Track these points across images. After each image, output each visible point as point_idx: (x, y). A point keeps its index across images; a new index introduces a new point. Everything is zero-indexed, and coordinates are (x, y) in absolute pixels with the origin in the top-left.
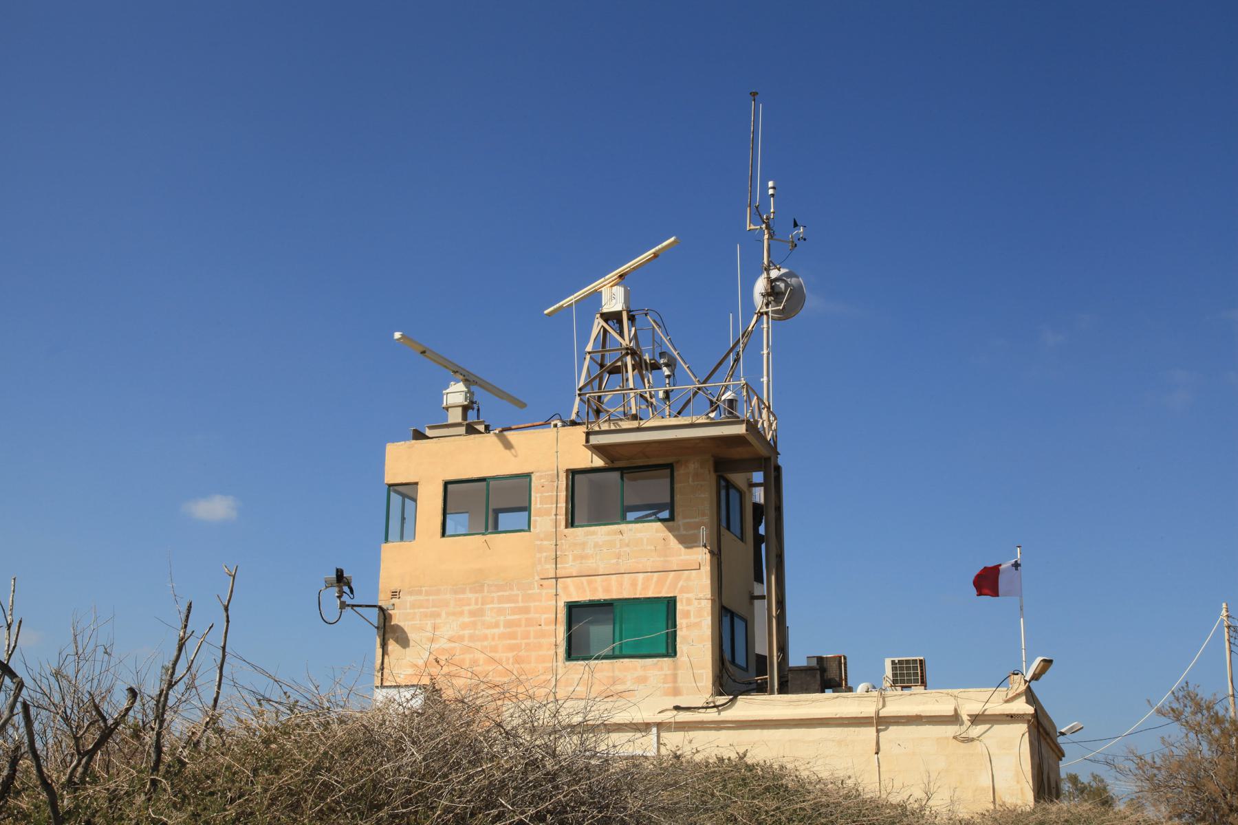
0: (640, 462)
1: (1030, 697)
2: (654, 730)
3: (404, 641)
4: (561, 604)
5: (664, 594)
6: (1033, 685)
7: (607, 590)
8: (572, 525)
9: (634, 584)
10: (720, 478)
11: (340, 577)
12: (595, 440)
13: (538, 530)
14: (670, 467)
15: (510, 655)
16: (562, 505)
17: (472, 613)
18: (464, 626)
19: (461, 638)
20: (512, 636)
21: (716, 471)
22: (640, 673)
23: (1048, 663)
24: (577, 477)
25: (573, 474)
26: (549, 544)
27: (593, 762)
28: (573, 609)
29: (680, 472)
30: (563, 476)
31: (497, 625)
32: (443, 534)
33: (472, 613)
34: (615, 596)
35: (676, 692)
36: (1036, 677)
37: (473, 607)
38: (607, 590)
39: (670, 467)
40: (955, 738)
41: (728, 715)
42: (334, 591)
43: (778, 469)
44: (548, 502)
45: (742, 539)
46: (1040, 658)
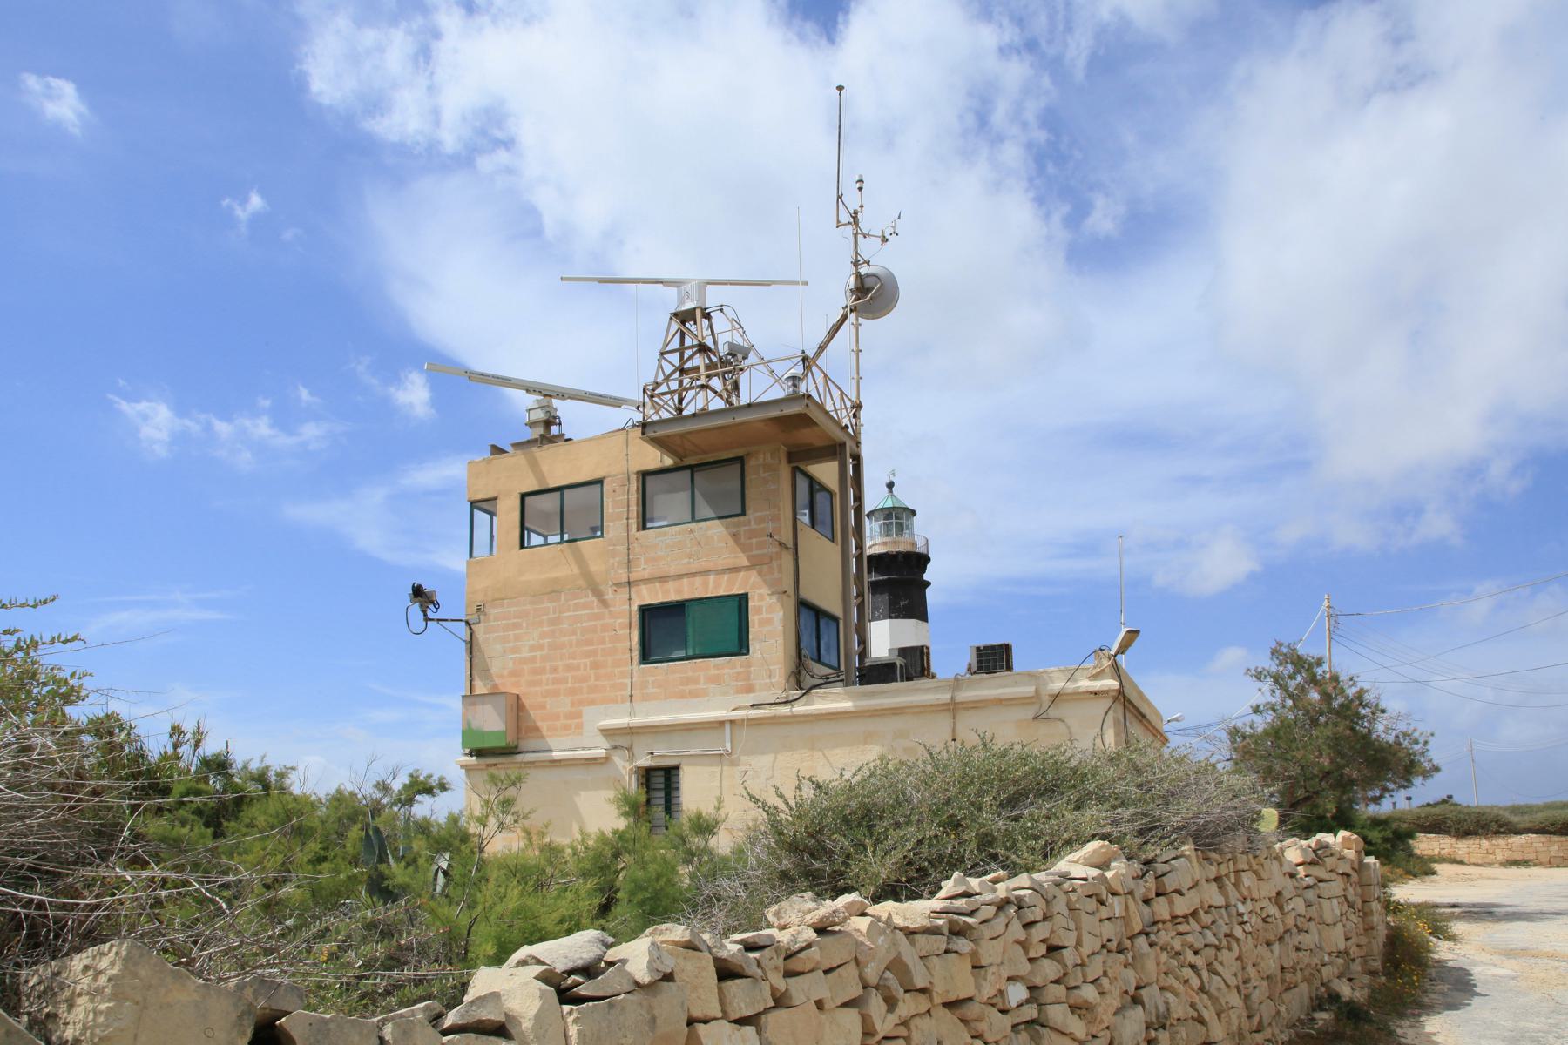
0: (710, 458)
1: (1117, 671)
2: (727, 726)
3: (1450, 797)
4: (635, 608)
5: (735, 592)
6: (1122, 660)
7: (763, 622)
8: (644, 528)
9: (706, 584)
10: (796, 471)
11: (417, 592)
12: (651, 434)
13: (611, 534)
14: (741, 460)
15: (587, 661)
16: (634, 508)
17: (552, 622)
18: (543, 636)
19: (541, 647)
20: (589, 642)
21: (790, 461)
22: (713, 672)
23: (1133, 634)
24: (649, 479)
25: (645, 475)
26: (622, 548)
27: (86, 762)
28: (647, 612)
29: (751, 464)
30: (633, 478)
31: (574, 633)
32: (522, 546)
33: (552, 622)
34: (687, 597)
35: (749, 689)
36: (1122, 650)
37: (551, 615)
38: (679, 591)
39: (741, 460)
40: (1035, 718)
41: (799, 708)
42: (416, 608)
43: (857, 458)
44: (619, 505)
45: (833, 541)
46: (1125, 630)
